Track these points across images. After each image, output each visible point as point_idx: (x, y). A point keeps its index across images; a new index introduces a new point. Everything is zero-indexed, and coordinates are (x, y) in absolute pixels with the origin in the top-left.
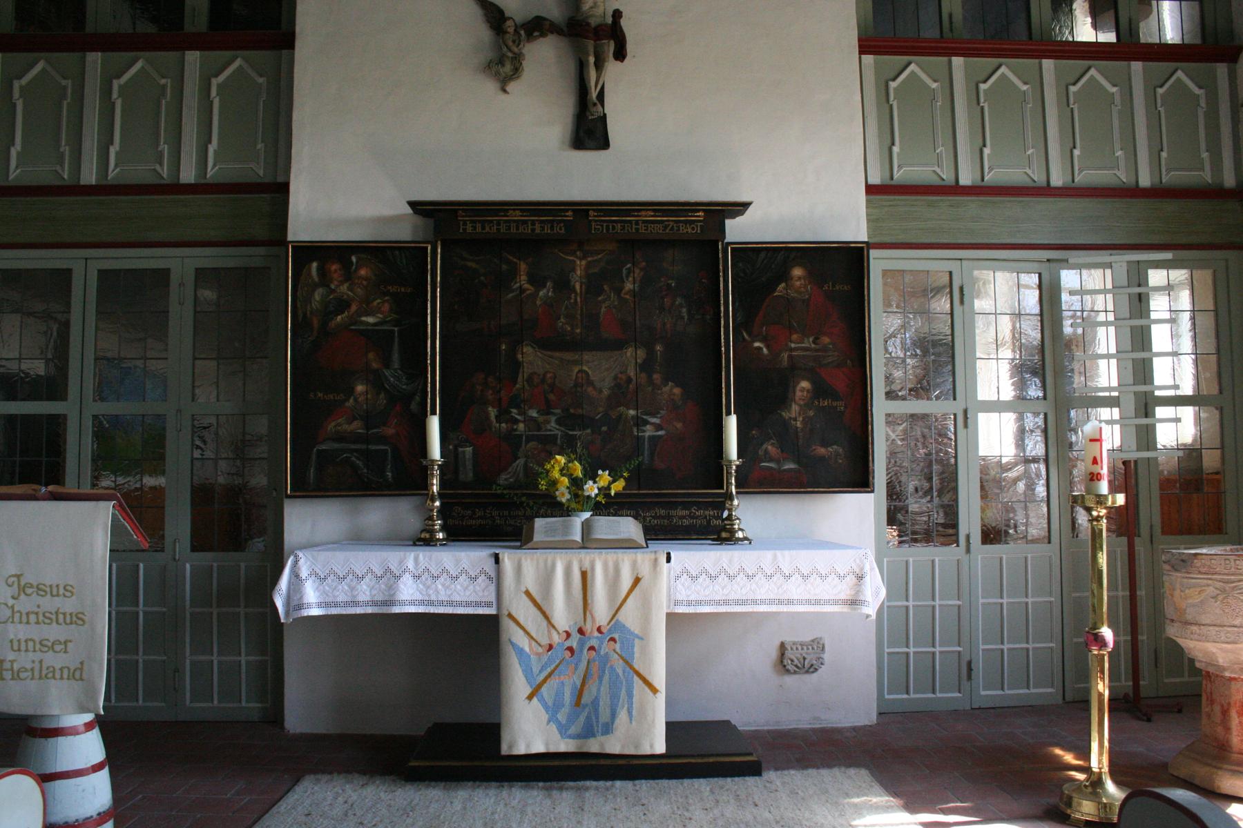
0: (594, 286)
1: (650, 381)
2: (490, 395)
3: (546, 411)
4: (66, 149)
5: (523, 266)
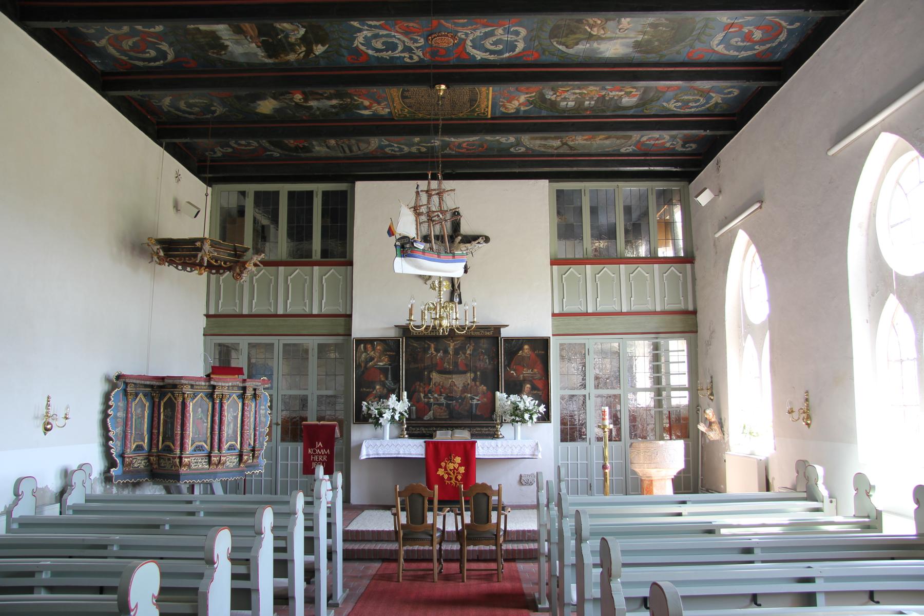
0: (456, 352)
4: (272, 301)
5: (432, 345)
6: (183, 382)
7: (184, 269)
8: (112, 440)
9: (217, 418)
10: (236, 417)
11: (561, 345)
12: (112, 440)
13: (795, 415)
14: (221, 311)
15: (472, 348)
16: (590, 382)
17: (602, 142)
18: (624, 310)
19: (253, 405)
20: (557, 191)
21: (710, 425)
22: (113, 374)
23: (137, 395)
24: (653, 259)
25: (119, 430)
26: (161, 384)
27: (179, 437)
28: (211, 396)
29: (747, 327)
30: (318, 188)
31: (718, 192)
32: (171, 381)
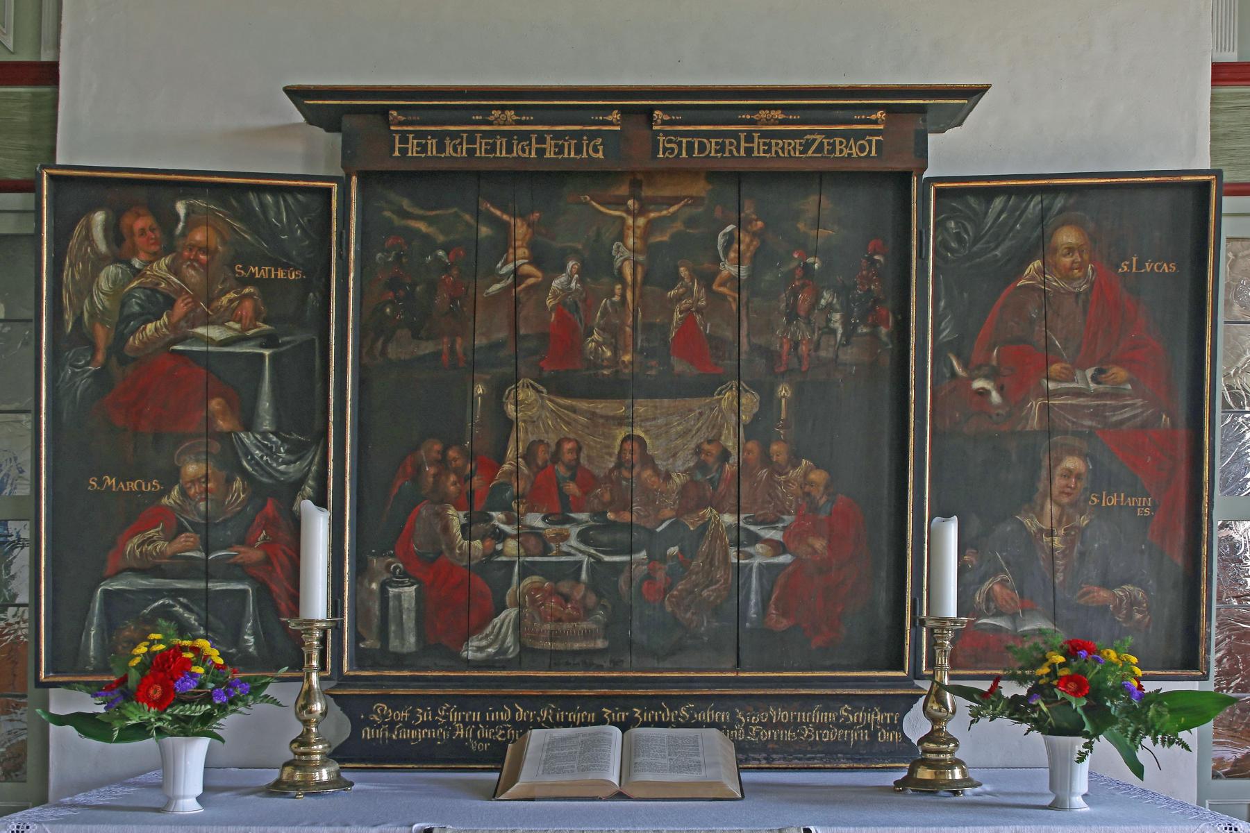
0: (658, 275)
2: (451, 484)
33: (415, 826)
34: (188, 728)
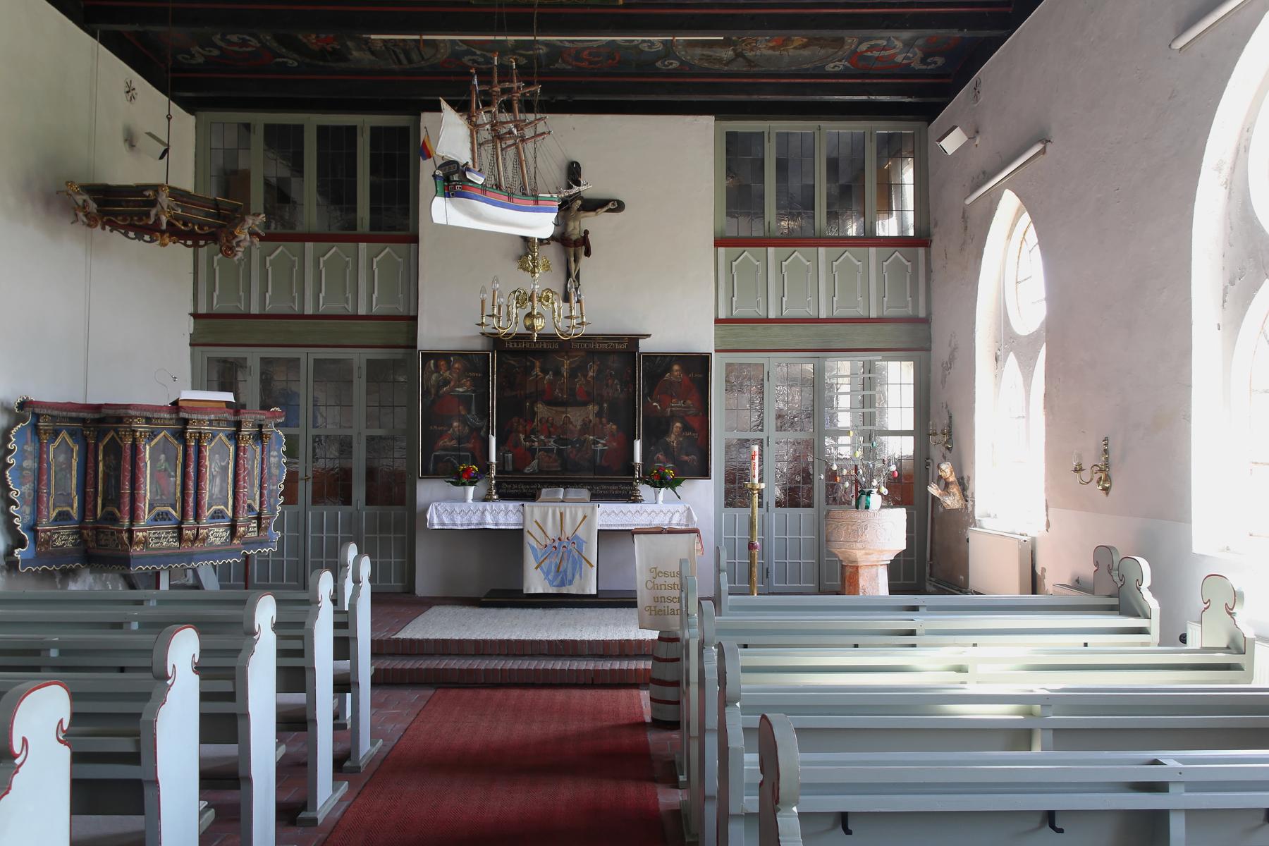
0: (573, 373)
1: (601, 422)
2: (521, 428)
3: (549, 437)
5: (538, 364)
6: (132, 412)
7: (139, 237)
8: (15, 503)
9: (191, 470)
10: (225, 469)
11: (728, 365)
12: (15, 503)
13: (1086, 475)
14: (216, 308)
15: (595, 367)
16: (770, 422)
17: (798, 52)
18: (823, 315)
19: (259, 449)
20: (728, 134)
21: (946, 486)
22: (14, 400)
23: (56, 433)
24: (869, 239)
25: (27, 488)
26: (97, 416)
27: (127, 500)
28: (181, 435)
29: (1008, 341)
30: (365, 122)
31: (974, 133)
32: (110, 412)
33: (1144, 564)
34: (472, 484)
